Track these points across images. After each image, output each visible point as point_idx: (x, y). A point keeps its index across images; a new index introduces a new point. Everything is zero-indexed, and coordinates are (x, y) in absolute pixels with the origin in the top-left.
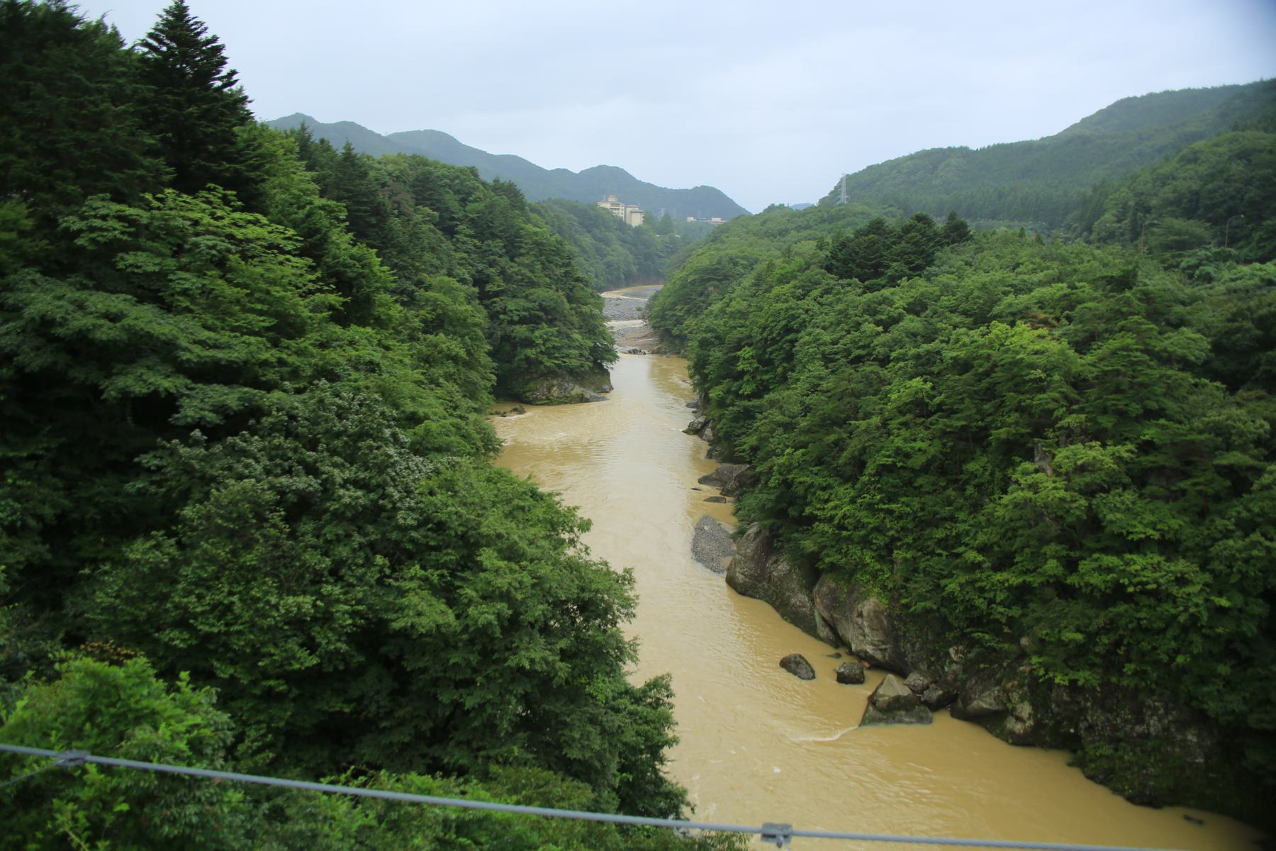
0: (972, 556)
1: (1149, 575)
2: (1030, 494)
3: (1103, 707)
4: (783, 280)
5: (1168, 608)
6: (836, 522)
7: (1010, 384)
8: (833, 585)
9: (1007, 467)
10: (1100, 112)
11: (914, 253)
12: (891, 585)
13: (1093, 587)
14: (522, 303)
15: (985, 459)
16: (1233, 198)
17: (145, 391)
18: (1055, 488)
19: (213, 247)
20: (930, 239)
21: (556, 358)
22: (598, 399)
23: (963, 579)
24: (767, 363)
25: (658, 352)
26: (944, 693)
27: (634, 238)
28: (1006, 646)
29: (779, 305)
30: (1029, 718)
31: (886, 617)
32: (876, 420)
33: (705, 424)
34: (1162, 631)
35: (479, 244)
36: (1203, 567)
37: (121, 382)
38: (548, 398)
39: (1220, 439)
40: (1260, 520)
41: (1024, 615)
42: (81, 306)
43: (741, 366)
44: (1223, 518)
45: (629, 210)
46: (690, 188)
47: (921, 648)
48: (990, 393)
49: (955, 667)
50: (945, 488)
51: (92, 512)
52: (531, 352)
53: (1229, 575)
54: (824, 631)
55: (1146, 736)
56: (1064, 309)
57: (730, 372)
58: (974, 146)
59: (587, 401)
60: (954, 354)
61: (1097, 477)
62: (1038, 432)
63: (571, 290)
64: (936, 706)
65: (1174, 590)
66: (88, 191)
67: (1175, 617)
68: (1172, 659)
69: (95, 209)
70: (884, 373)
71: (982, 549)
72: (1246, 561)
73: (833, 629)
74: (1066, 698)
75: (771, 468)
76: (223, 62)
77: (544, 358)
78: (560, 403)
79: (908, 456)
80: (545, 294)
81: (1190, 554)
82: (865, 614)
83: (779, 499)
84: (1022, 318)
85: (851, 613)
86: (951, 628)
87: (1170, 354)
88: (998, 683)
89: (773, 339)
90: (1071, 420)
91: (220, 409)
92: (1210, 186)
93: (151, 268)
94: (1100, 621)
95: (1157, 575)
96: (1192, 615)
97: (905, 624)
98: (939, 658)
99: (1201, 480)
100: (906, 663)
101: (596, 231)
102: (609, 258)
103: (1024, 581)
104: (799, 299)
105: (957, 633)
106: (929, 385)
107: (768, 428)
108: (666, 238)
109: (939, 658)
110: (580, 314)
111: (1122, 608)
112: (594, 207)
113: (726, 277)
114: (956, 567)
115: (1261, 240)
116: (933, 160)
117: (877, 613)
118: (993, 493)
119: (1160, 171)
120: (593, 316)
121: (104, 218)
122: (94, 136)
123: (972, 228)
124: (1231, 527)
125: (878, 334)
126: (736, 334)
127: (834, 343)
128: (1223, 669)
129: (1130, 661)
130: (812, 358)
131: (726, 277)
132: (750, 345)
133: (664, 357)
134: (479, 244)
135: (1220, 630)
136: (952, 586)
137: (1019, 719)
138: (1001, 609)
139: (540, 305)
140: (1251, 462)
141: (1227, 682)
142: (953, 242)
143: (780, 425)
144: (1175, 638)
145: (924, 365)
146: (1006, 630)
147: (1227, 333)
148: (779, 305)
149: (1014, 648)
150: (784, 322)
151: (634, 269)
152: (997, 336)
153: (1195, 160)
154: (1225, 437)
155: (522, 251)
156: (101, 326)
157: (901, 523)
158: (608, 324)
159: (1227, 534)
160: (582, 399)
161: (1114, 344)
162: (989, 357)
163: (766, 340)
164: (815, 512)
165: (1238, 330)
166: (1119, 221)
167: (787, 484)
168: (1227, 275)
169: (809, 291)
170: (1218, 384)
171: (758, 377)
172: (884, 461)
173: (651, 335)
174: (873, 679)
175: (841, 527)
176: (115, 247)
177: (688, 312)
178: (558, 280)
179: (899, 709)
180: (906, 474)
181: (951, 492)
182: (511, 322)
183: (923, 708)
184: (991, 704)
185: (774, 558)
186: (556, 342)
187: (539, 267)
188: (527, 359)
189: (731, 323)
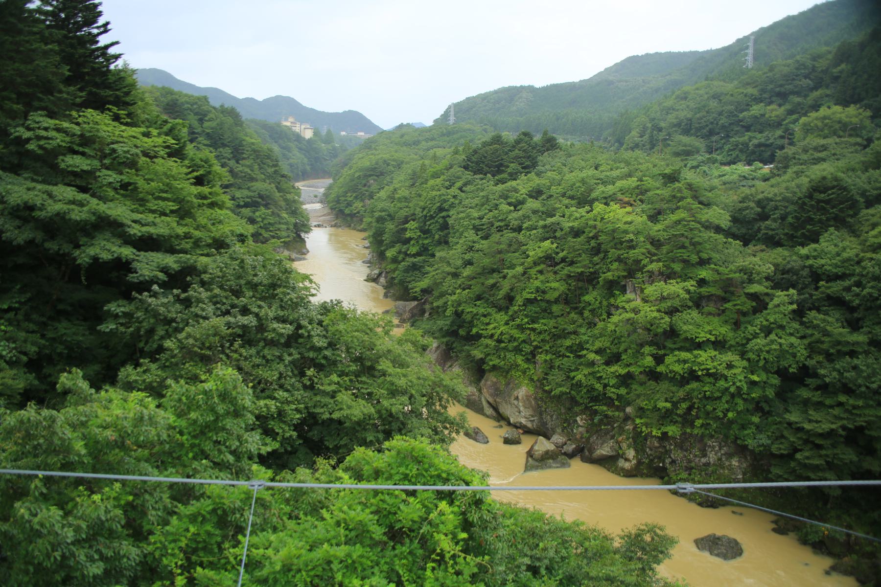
0: (592, 356)
1: (710, 365)
2: (633, 315)
3: (681, 448)
4: (435, 176)
5: (722, 383)
6: (496, 337)
7: (612, 244)
8: (495, 380)
9: (610, 297)
10: (616, 65)
11: (524, 157)
12: (536, 378)
13: (676, 373)
14: (246, 193)
15: (595, 293)
16: (712, 123)
17: (110, 257)
18: (652, 311)
19: (128, 152)
20: (533, 148)
21: (271, 231)
22: (300, 259)
23: (586, 372)
24: (425, 232)
25: (335, 226)
27: (308, 147)
28: (617, 413)
29: (434, 193)
32: (520, 269)
33: (380, 275)
34: (719, 398)
36: (743, 355)
37: (92, 251)
39: (746, 277)
40: (772, 326)
41: (628, 393)
42: (50, 195)
43: (408, 235)
44: (752, 326)
45: (303, 127)
46: (341, 111)
47: (557, 418)
48: (597, 251)
49: (581, 429)
50: (569, 313)
51: (60, 348)
53: (758, 361)
54: (489, 411)
55: (707, 464)
56: (638, 195)
57: (400, 239)
58: (538, 85)
60: (571, 224)
61: (677, 303)
62: (631, 274)
63: (279, 183)
64: (571, 456)
65: (725, 372)
66: (30, 107)
67: (727, 389)
68: (725, 415)
69: (38, 123)
70: (521, 237)
71: (598, 352)
72: (768, 352)
73: (496, 409)
74: (656, 444)
75: (446, 303)
76: (100, 14)
77: (263, 232)
79: (544, 292)
80: (262, 186)
81: (733, 349)
82: (520, 398)
83: (453, 323)
84: (612, 200)
85: (510, 397)
86: (577, 403)
87: (711, 223)
88: (613, 437)
89: (431, 216)
90: (654, 267)
91: (164, 270)
92: (698, 116)
93: (85, 168)
94: (681, 393)
95: (715, 364)
96: (738, 387)
97: (545, 403)
98: (569, 424)
99: (739, 302)
100: (547, 429)
101: (281, 141)
102: (291, 161)
103: (629, 372)
104: (448, 189)
105: (583, 407)
106: (555, 245)
107: (441, 276)
108: (330, 147)
109: (569, 424)
110: (286, 200)
111: (694, 385)
112: (279, 125)
113: (382, 174)
114: (581, 364)
115: (730, 150)
116: (510, 95)
117: (528, 397)
118: (601, 315)
119: (665, 104)
120: (294, 201)
121: (46, 129)
122: (29, 67)
123: (560, 141)
124: (758, 331)
125: (511, 211)
126: (403, 213)
127: (481, 218)
128: (756, 419)
129: (698, 418)
130: (466, 228)
131: (382, 174)
132: (414, 220)
133: (340, 229)
135: (753, 395)
136: (579, 377)
137: (627, 460)
138: (613, 390)
139: (259, 194)
140: (766, 291)
141: (757, 427)
142: (548, 150)
143: (448, 274)
144: (727, 402)
145: (550, 233)
146: (617, 403)
147: (740, 210)
148: (434, 193)
149: (622, 414)
150: (438, 204)
151: (308, 168)
152: (599, 213)
153: (685, 98)
154: (749, 276)
155: (244, 156)
156: (73, 210)
157: (542, 337)
158: (304, 207)
159: (755, 336)
161: (674, 217)
162: (595, 227)
163: (426, 216)
164: (481, 332)
165: (747, 208)
166: (641, 137)
167: (458, 314)
168: (716, 173)
169: (454, 183)
170: (738, 242)
171: (421, 242)
172: (529, 296)
173: (328, 214)
174: (527, 442)
175: (499, 341)
176: (56, 152)
177: (356, 198)
178: (270, 177)
179: (548, 459)
180: (544, 305)
181: (573, 315)
183: (563, 457)
185: (449, 364)
186: (272, 220)
187: (256, 167)
189: (399, 205)
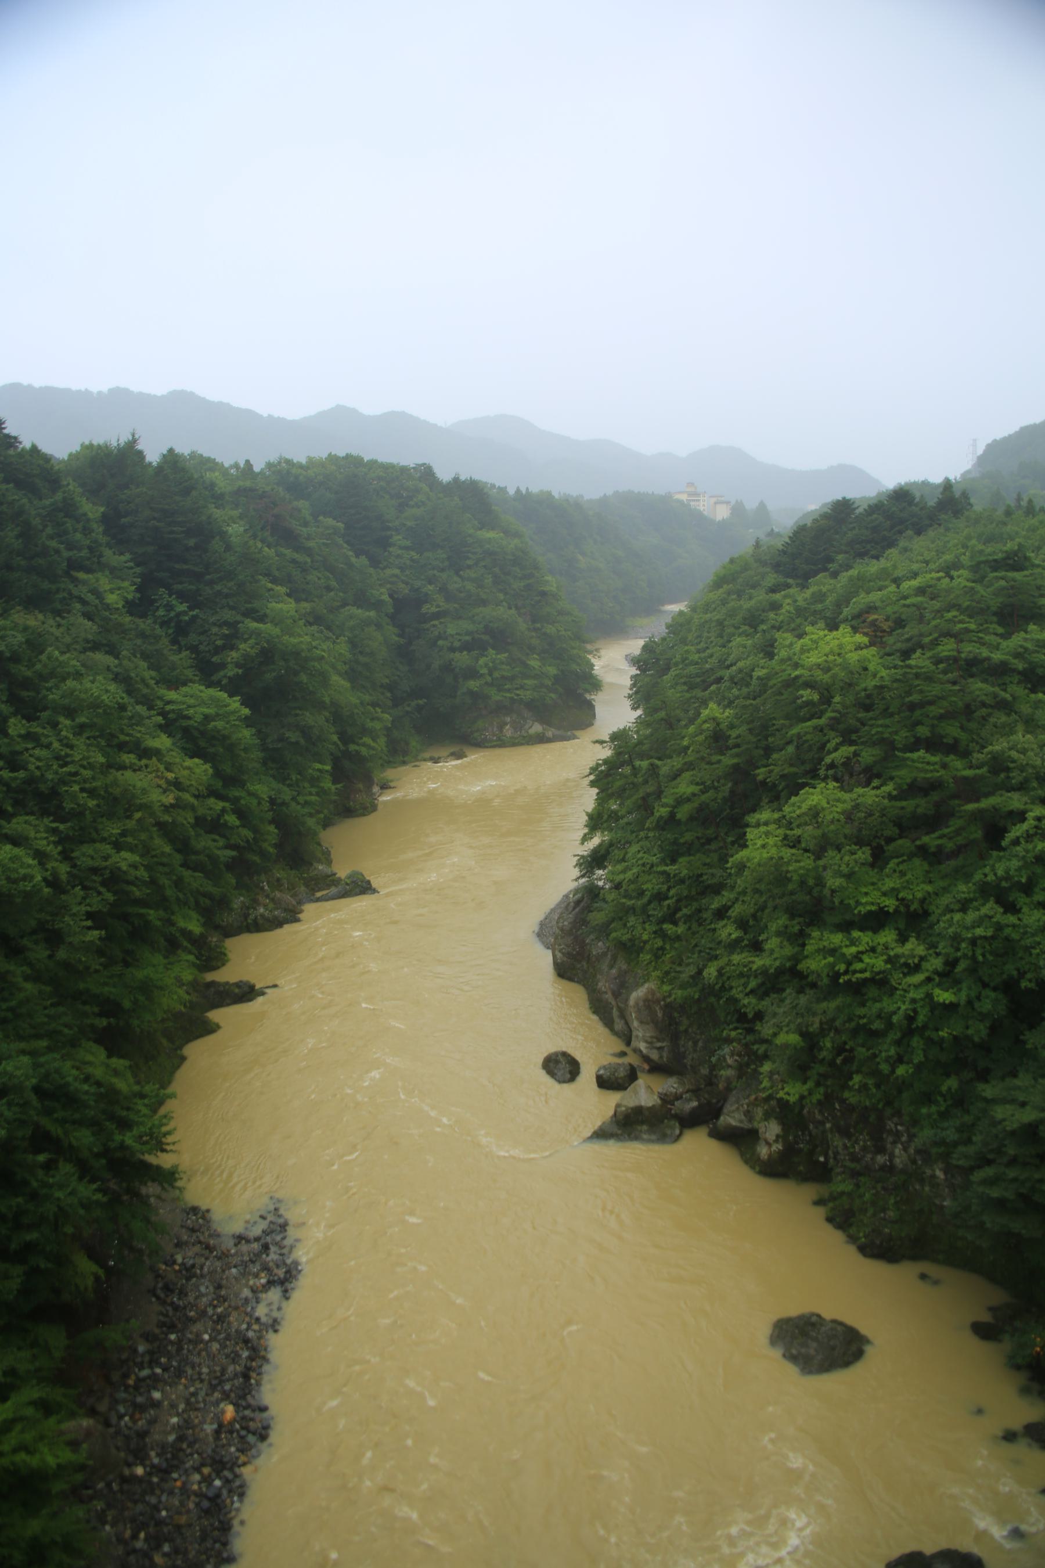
8: (624, 967)
14: (466, 625)
21: (509, 691)
26: (700, 1106)
30: (776, 1141)
31: (661, 1008)
35: (416, 557)
38: (499, 739)
52: (473, 684)
59: (549, 740)
64: (689, 1122)
78: (514, 745)
80: (500, 613)
134: (416, 557)
155: (469, 562)
160: (541, 739)
179: (642, 1123)
182: (452, 649)
184: (741, 1121)
188: (472, 693)
